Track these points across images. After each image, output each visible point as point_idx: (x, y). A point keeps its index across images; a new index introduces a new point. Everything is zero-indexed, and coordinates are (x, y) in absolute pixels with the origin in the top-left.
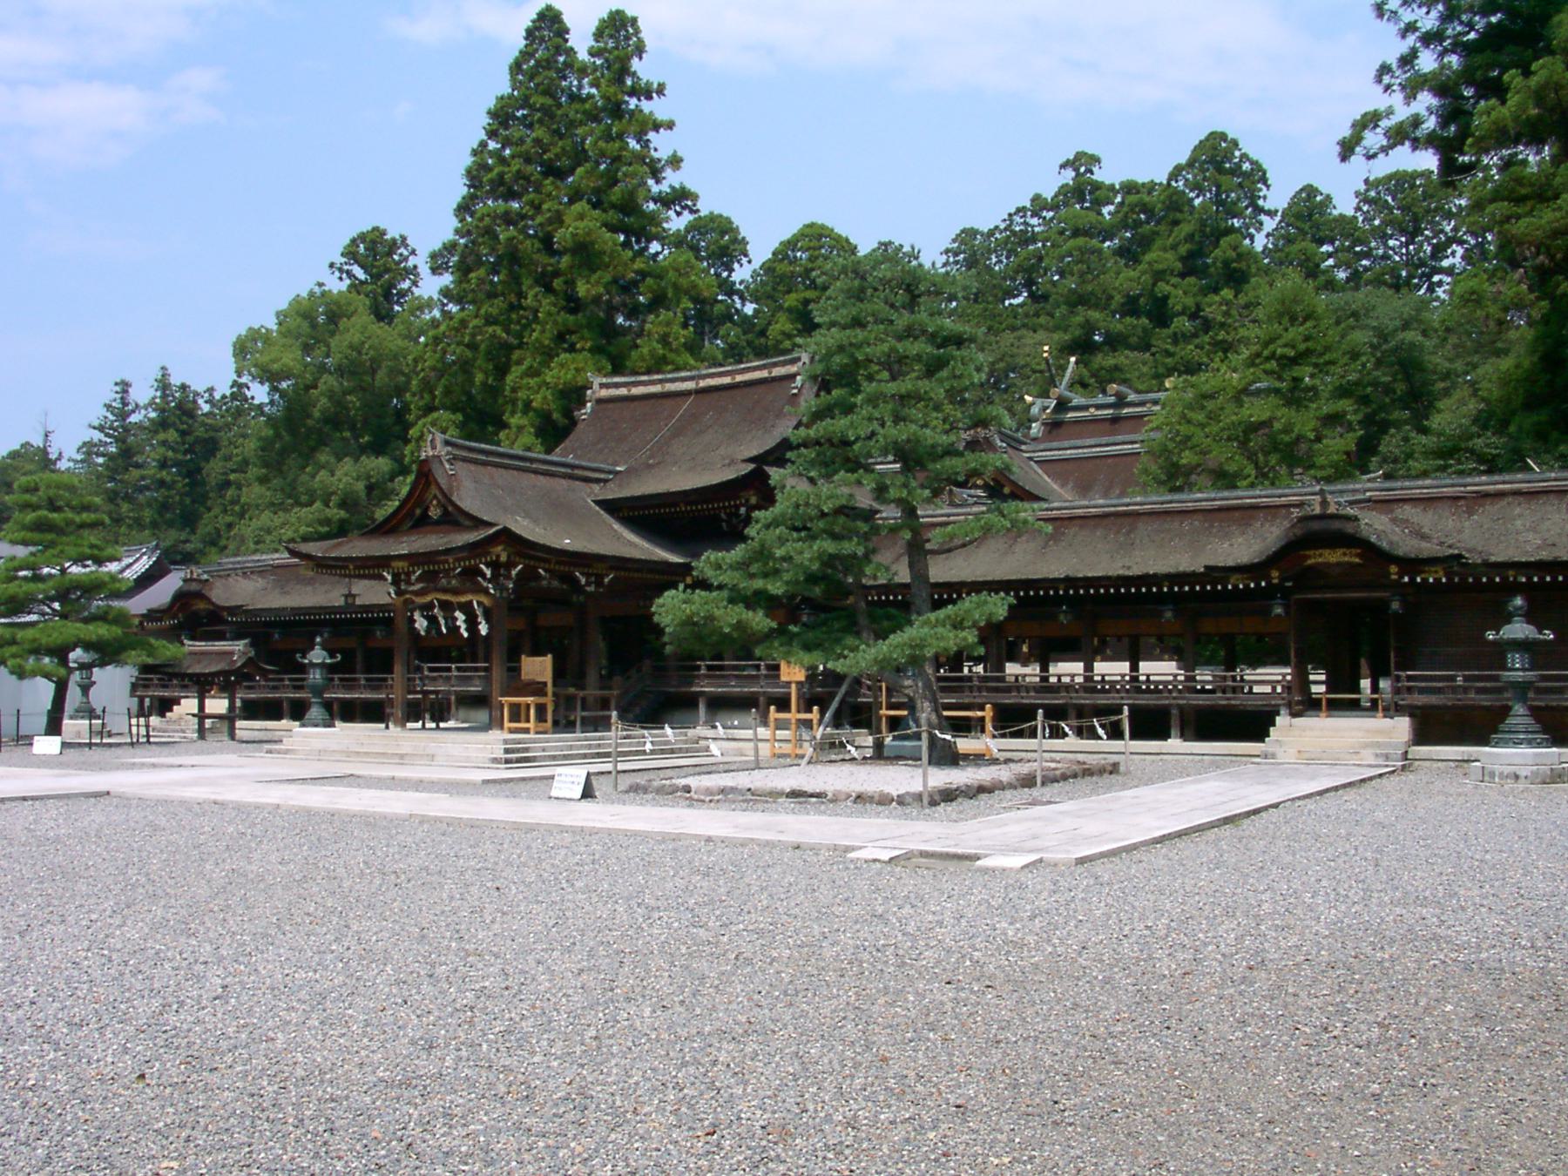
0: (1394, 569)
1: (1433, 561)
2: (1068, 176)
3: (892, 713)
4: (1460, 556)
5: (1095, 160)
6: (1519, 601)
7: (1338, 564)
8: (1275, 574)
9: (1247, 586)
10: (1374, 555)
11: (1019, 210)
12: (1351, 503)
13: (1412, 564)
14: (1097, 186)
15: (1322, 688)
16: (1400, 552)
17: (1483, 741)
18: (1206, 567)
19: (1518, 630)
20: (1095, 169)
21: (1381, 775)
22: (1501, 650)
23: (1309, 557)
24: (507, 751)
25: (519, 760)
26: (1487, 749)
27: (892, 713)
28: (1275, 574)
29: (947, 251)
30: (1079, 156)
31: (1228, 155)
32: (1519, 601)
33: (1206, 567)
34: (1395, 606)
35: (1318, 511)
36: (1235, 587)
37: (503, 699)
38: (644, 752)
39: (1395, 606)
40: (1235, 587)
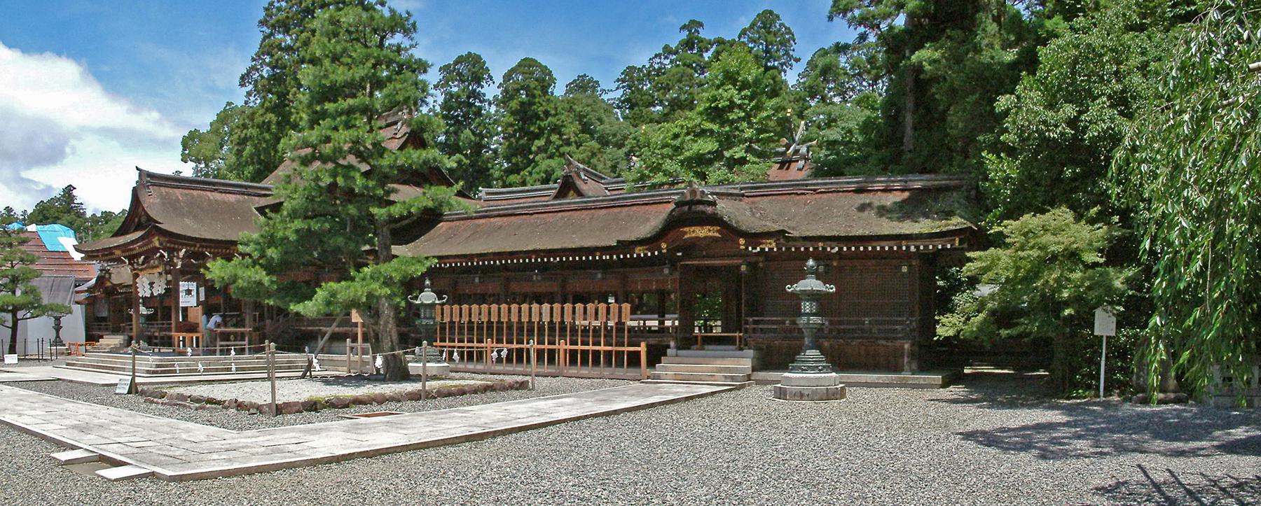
0: (742, 241)
1: (768, 235)
2: (684, 35)
3: (632, 349)
4: (784, 232)
5: (701, 25)
6: (811, 262)
7: (705, 238)
8: (664, 246)
9: (646, 255)
10: (731, 231)
11: (656, 56)
12: (712, 194)
13: (754, 238)
14: (701, 41)
15: (719, 329)
16: (744, 228)
17: (783, 367)
18: (619, 242)
19: (811, 284)
20: (700, 30)
21: (713, 393)
22: (797, 297)
23: (686, 233)
24: (158, 366)
25: (163, 372)
26: (786, 374)
27: (632, 349)
28: (664, 246)
29: (618, 80)
30: (692, 22)
31: (773, 22)
32: (811, 262)
33: (619, 242)
34: (743, 268)
35: (689, 198)
36: (639, 255)
37: (643, 344)
38: (175, 371)
39: (743, 268)
40: (639, 255)
